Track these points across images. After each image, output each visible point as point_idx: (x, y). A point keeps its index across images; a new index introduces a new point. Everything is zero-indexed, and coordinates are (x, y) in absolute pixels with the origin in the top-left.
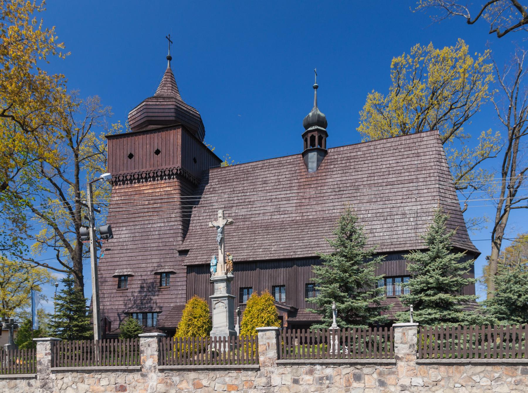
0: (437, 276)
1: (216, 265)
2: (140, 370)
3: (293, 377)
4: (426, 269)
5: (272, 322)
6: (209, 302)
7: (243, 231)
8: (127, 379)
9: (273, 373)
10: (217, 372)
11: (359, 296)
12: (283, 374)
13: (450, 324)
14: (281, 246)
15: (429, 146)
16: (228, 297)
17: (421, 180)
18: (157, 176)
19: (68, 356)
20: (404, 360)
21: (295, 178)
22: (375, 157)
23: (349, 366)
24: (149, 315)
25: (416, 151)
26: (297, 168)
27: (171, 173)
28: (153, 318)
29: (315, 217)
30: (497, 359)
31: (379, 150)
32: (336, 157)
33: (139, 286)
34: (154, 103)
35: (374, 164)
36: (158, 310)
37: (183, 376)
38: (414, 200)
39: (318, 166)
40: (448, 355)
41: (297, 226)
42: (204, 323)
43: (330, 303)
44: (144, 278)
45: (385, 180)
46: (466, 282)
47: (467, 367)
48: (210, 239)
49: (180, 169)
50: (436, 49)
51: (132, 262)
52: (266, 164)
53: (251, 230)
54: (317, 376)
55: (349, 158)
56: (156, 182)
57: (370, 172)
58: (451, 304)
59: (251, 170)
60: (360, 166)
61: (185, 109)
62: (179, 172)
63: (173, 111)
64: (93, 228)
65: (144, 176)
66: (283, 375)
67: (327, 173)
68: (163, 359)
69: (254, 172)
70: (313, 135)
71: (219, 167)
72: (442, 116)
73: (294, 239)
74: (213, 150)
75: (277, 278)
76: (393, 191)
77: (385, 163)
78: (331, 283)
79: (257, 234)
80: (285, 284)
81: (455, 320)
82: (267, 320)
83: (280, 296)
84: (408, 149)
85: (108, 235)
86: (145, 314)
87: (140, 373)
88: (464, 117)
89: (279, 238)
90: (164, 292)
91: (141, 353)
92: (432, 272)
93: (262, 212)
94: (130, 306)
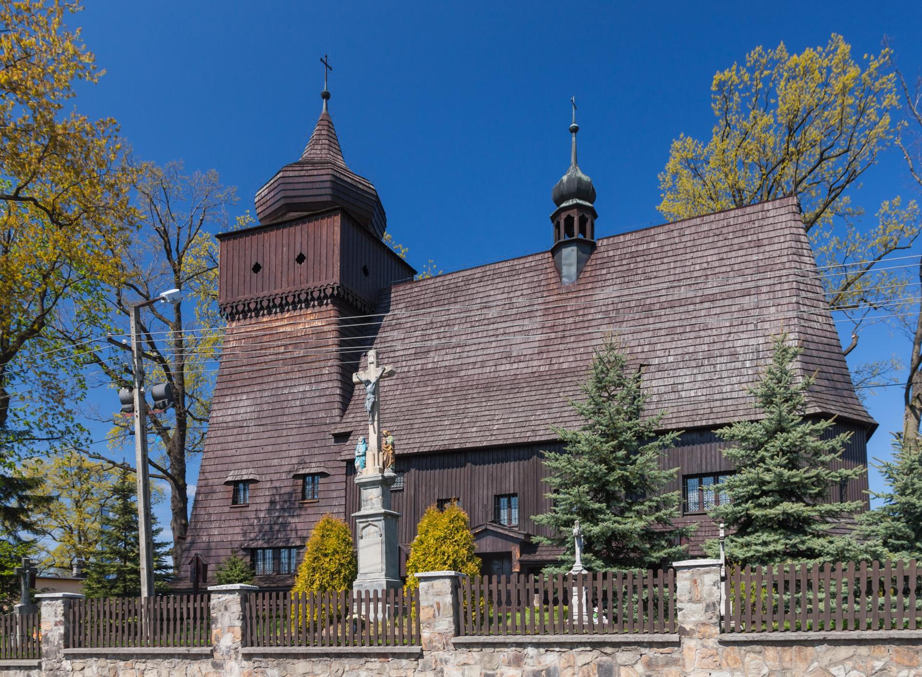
0: (778, 470)
1: (365, 455)
2: (210, 656)
3: (484, 671)
4: (758, 456)
5: (462, 561)
6: (352, 523)
7: (446, 395)
8: (188, 672)
9: (446, 662)
10: (345, 661)
11: (630, 510)
12: (465, 664)
13: (804, 561)
14: (510, 420)
15: (779, 226)
16: (385, 515)
17: (765, 289)
18: (300, 302)
19: (117, 628)
20: (696, 635)
21: (539, 295)
22: (681, 251)
23: (589, 648)
24: (284, 554)
25: (755, 237)
26: (542, 277)
27: (322, 295)
28: (290, 558)
29: (573, 365)
30: (881, 632)
31: (688, 238)
32: (611, 253)
33: (268, 499)
34: (297, 173)
35: (678, 264)
36: (298, 543)
37: (285, 668)
38: (751, 327)
39: (579, 271)
40: (781, 624)
41: (541, 383)
42: (342, 565)
43: (569, 523)
44: (277, 484)
45: (700, 293)
46: (837, 477)
47: (818, 648)
48: (387, 411)
49: (338, 287)
50: (791, 54)
51: (255, 457)
52: (488, 273)
53: (458, 393)
54: (528, 668)
55: (634, 256)
56: (297, 313)
57: (672, 278)
58: (808, 521)
59: (463, 284)
60: (654, 269)
61: (349, 180)
62: (336, 292)
63: (328, 185)
64: (140, 388)
65: (278, 301)
66: (466, 667)
67: (595, 285)
68: (252, 635)
69: (468, 287)
70: (569, 216)
71: (411, 281)
72: (816, 179)
73: (533, 408)
74: (402, 254)
75: (504, 481)
76: (713, 311)
77: (699, 261)
78: (576, 483)
79: (469, 401)
80: (517, 491)
81: (811, 554)
82: (451, 558)
83: (510, 515)
84: (740, 234)
85: (166, 400)
86: (277, 550)
87: (210, 660)
88: (847, 175)
89: (507, 406)
90: (310, 511)
91: (213, 623)
92: (768, 461)
93: (480, 359)
94: (252, 535)
